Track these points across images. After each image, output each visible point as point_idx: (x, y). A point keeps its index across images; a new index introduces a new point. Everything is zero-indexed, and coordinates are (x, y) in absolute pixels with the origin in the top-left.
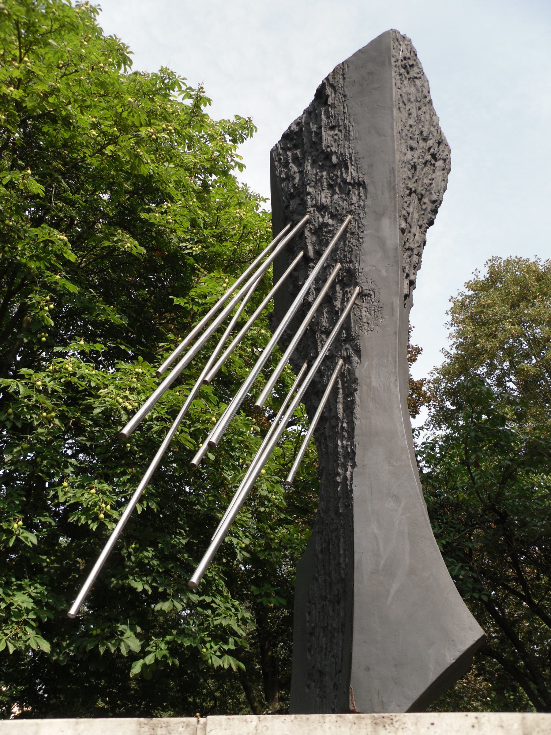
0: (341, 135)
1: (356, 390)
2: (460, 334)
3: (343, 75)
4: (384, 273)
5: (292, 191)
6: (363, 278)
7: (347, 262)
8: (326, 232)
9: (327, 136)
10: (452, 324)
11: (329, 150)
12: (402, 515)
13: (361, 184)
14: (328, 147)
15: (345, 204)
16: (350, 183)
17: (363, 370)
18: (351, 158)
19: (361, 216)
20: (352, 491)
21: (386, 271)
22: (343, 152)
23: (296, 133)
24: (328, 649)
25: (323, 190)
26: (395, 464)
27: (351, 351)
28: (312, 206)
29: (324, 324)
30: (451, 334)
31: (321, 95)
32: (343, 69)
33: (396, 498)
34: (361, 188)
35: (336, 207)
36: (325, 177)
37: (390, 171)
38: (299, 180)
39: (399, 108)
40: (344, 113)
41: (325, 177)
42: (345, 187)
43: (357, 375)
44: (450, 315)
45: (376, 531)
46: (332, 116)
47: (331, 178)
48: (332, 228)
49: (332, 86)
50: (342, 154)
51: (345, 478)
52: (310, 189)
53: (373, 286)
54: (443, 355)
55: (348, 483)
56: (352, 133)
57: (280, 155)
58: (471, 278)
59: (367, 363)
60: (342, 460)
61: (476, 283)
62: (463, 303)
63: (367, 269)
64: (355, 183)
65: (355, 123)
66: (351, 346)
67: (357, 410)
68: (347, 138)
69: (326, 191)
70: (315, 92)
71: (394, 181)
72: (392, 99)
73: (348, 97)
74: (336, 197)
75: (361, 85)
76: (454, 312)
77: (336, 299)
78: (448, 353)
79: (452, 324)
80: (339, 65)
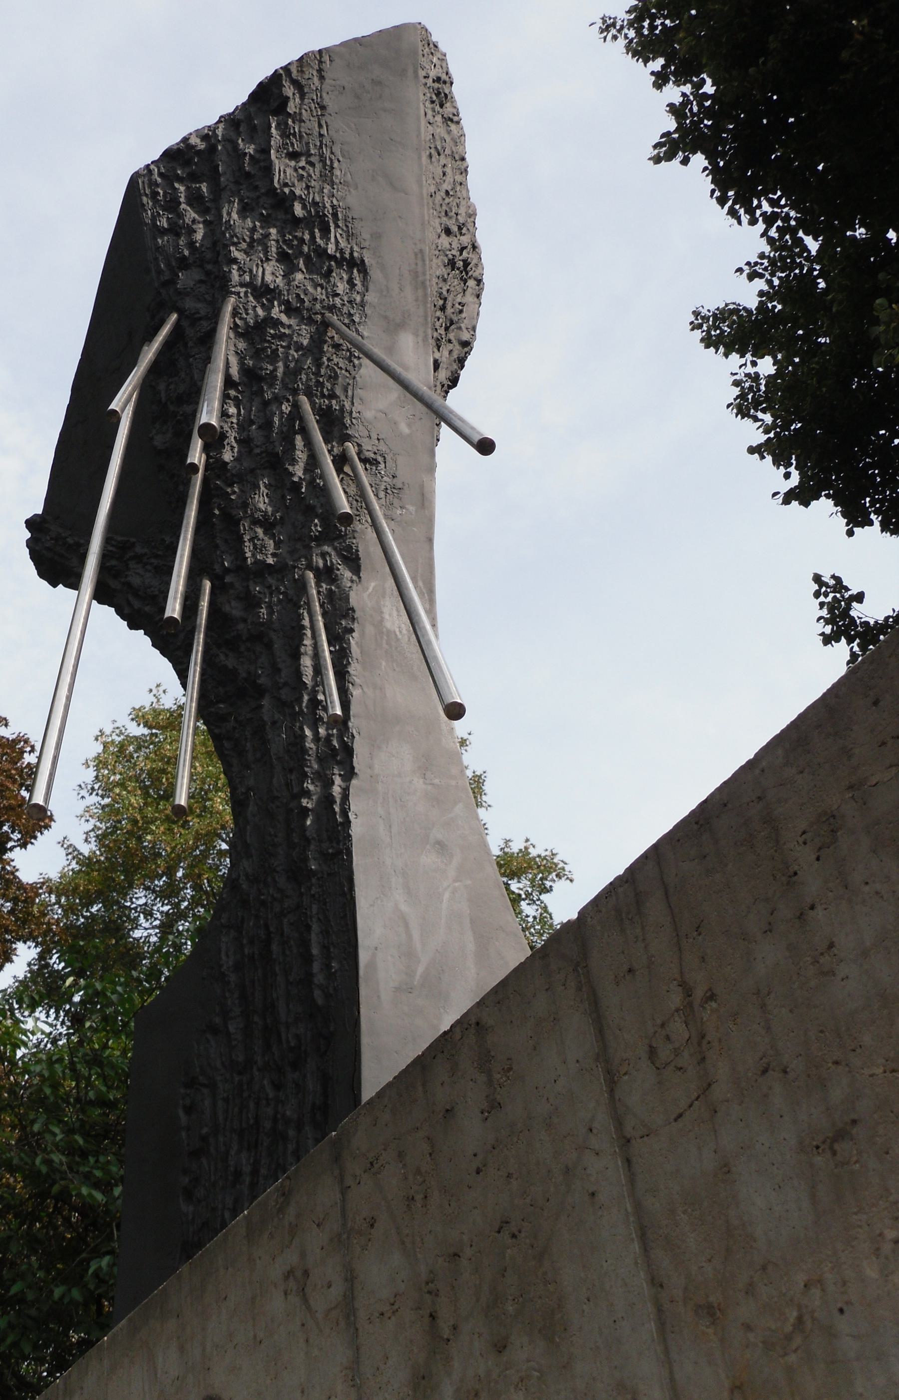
0: (315, 173)
1: (352, 631)
2: (108, 812)
3: (320, 71)
4: (404, 428)
5: (186, 253)
6: (361, 428)
7: (323, 396)
8: (273, 336)
9: (283, 169)
10: (93, 789)
11: (287, 190)
12: (455, 881)
13: (355, 264)
14: (286, 185)
15: (319, 293)
16: (332, 257)
17: (365, 595)
18: (335, 215)
19: (356, 319)
20: (347, 823)
21: (409, 426)
22: (317, 199)
23: (199, 153)
24: (263, 1171)
25: (268, 260)
26: (436, 781)
27: (336, 560)
28: (242, 285)
29: (262, 506)
30: (87, 810)
31: (268, 96)
32: (320, 62)
33: (441, 847)
34: (355, 271)
35: (298, 295)
36: (274, 237)
37: (416, 255)
38: (204, 237)
39: (430, 156)
40: (321, 135)
41: (274, 237)
42: (321, 263)
43: (353, 602)
44: (92, 769)
45: (403, 907)
46: (294, 135)
47: (288, 243)
48: (287, 331)
49: (296, 84)
50: (315, 204)
51: (328, 800)
52: (236, 254)
53: (382, 447)
54: (64, 852)
55: (337, 809)
56: (337, 172)
57: (157, 185)
58: (146, 701)
59: (373, 584)
60: (316, 766)
61: (156, 712)
62: (122, 747)
63: (368, 414)
64: (343, 258)
65: (343, 156)
66: (335, 549)
67: (354, 669)
68: (327, 177)
69: (273, 263)
70: (253, 87)
71: (424, 274)
72: (419, 135)
73: (330, 109)
74: (299, 276)
75: (358, 97)
76: (100, 763)
77: (294, 462)
78: (75, 849)
79: (93, 789)
80: (313, 52)
